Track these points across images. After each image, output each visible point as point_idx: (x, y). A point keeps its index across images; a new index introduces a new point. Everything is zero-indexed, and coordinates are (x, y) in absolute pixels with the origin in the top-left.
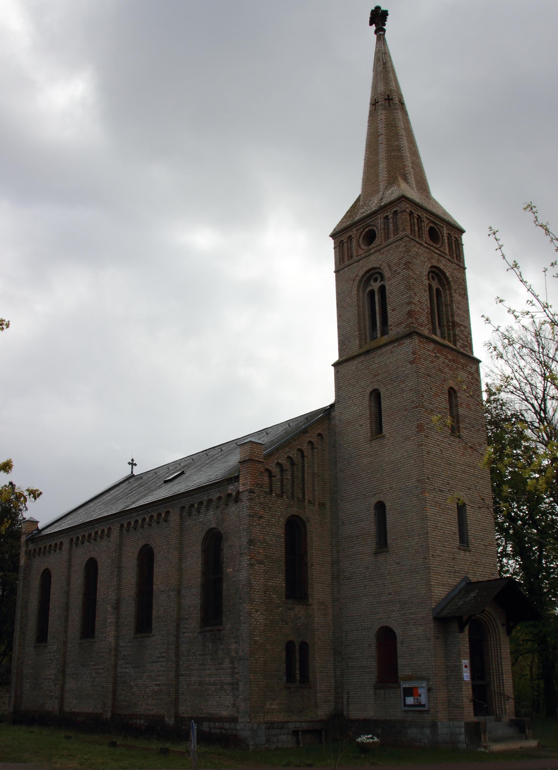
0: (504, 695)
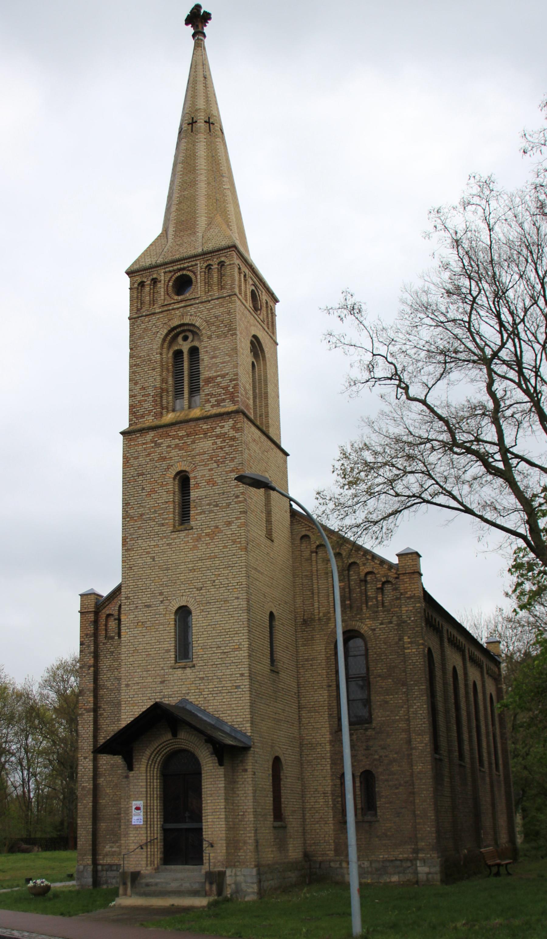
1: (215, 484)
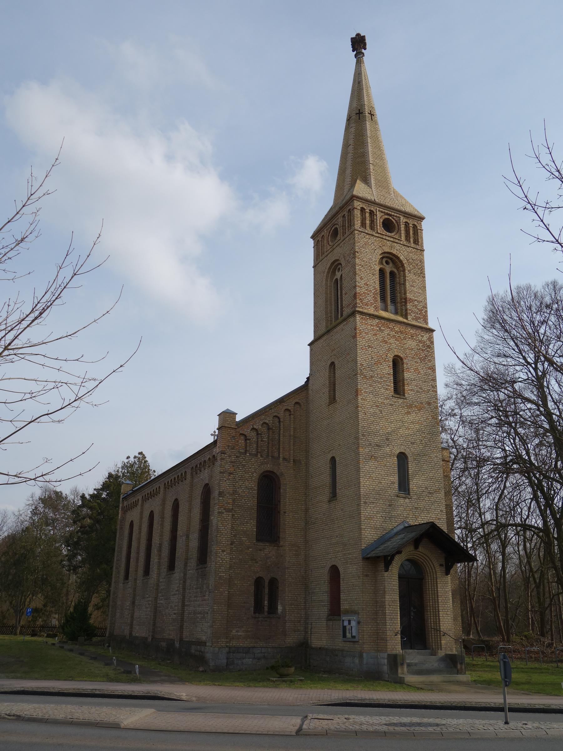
0: (440, 631)
1: (419, 373)
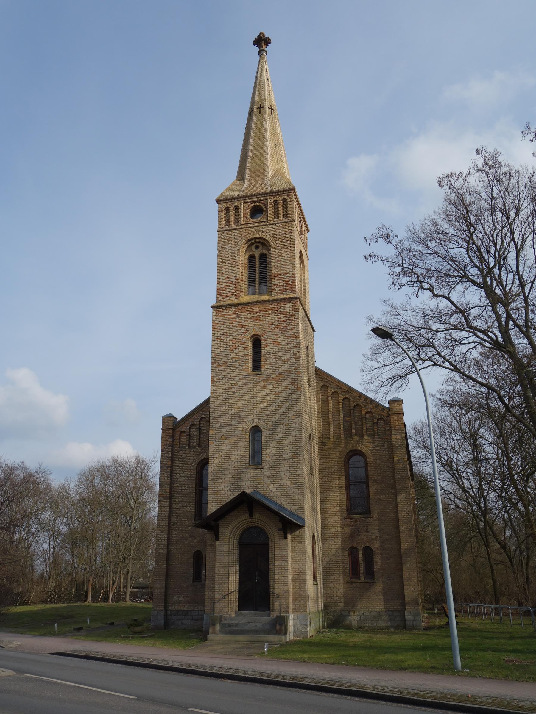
1: (279, 344)
